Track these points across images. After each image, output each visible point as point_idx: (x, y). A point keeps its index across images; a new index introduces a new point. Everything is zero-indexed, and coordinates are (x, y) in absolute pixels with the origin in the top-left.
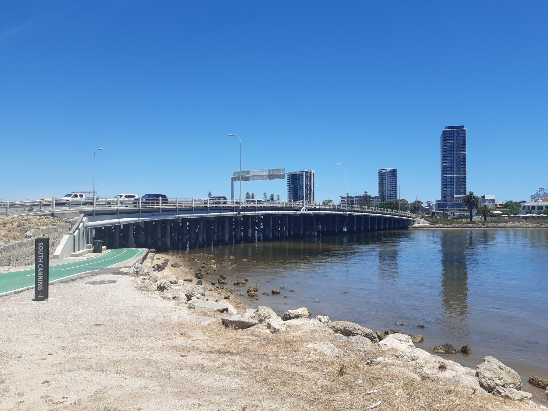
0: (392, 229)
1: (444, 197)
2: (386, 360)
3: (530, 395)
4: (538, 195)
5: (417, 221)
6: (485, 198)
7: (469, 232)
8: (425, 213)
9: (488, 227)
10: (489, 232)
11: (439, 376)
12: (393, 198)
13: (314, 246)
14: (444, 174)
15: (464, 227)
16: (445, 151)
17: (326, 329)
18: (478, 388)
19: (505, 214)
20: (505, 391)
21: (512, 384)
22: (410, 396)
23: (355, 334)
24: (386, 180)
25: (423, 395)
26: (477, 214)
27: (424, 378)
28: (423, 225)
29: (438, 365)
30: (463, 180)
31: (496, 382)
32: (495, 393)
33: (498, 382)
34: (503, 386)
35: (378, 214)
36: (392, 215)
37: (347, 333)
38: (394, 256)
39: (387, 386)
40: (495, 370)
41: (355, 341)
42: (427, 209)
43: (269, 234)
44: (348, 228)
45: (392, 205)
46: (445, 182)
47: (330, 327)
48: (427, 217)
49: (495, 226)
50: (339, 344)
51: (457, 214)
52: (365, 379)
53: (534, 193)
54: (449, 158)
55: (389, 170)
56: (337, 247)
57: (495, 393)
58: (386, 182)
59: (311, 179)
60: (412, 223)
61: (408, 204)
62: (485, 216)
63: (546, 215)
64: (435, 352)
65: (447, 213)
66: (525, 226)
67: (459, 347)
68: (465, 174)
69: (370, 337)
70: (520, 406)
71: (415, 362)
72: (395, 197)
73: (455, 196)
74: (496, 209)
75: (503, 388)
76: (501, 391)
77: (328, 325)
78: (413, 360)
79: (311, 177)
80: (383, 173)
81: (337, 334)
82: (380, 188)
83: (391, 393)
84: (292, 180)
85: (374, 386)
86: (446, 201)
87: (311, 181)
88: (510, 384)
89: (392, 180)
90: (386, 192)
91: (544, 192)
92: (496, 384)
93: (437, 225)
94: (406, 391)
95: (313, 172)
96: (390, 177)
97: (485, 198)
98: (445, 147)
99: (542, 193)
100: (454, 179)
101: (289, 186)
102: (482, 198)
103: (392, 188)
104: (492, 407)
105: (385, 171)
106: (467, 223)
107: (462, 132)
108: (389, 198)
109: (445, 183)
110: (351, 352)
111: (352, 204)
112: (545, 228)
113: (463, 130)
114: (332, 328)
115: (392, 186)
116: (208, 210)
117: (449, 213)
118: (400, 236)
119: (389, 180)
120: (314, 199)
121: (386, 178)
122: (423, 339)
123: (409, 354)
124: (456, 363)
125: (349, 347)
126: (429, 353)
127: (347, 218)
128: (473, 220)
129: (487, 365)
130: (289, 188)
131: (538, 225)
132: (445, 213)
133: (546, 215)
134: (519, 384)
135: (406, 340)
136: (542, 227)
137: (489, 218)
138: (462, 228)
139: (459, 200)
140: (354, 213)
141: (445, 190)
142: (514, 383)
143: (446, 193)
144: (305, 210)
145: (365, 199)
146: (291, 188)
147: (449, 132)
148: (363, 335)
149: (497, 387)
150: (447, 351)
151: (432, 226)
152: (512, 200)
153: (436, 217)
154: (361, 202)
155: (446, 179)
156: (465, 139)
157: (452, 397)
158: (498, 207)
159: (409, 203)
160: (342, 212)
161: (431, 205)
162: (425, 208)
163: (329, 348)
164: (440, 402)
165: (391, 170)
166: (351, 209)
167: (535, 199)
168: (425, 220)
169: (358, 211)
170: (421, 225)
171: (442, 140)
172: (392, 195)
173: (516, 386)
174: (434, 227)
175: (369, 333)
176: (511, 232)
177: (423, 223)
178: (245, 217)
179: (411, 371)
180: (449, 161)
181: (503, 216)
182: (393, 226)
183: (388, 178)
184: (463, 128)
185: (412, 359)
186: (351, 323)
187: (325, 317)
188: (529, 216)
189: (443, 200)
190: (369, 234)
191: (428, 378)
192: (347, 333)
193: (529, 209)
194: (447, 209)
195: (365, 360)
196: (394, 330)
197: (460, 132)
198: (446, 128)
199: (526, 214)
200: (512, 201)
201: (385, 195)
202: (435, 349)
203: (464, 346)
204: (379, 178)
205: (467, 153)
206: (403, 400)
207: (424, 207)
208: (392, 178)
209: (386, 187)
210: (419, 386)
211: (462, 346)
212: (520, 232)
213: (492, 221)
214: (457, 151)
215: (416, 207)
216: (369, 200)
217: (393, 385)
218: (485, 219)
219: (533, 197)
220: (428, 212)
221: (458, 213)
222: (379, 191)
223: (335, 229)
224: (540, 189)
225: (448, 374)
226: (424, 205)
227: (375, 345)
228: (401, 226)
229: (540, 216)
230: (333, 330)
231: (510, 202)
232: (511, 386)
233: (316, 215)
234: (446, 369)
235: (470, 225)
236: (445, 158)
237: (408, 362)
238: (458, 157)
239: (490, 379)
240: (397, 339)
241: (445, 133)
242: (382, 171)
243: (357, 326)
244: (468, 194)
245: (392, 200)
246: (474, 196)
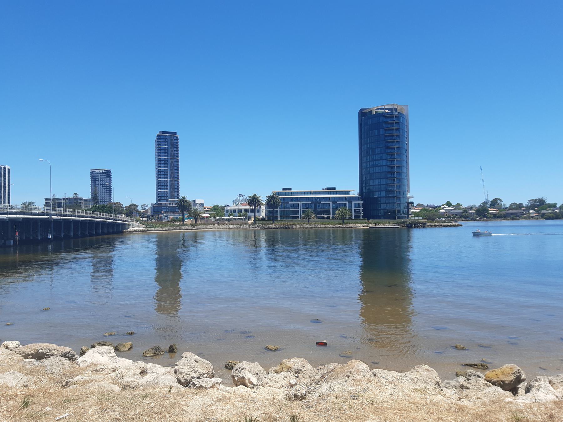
0: (100, 235)
1: (159, 200)
2: (85, 377)
3: (220, 380)
4: (238, 200)
5: (132, 225)
6: (196, 202)
7: (182, 234)
8: (140, 216)
9: (198, 229)
10: (199, 234)
11: (139, 382)
12: (107, 198)
13: (11, 258)
14: (158, 178)
15: (176, 230)
16: (160, 156)
17: (13, 356)
18: (176, 385)
19: (212, 217)
20: (200, 382)
21: (206, 373)
22: (104, 411)
23: (50, 356)
24: (100, 181)
25: (119, 406)
26: (189, 217)
27: (125, 387)
28: (138, 229)
29: (139, 371)
31: (192, 376)
32: (191, 386)
33: (194, 375)
34: (198, 378)
35: (89, 218)
36: (105, 219)
37: (39, 356)
38: (109, 262)
39: (80, 406)
40: (191, 364)
41: (49, 364)
42: (143, 213)
44: (53, 234)
45: (106, 208)
46: (159, 186)
47: (18, 354)
48: (142, 220)
49: (204, 228)
50: (29, 371)
51: (171, 217)
52: (56, 404)
53: (235, 198)
54: (163, 162)
55: (103, 171)
56: (41, 257)
57: (191, 386)
58: (100, 184)
59: (5, 176)
60: (127, 227)
61: (123, 207)
62: (196, 219)
63: (244, 218)
64: (144, 357)
65: (162, 217)
66: (228, 227)
67: (165, 347)
68: (178, 178)
69: (69, 356)
70: (209, 393)
71: (116, 372)
73: (169, 200)
74: (205, 213)
75: (198, 380)
76: (196, 383)
77: (16, 352)
78: (114, 371)
79: (5, 174)
80: (96, 174)
81: (27, 360)
82: (93, 190)
83: (84, 412)
85: (65, 410)
86: (161, 204)
87: (5, 189)
88: (204, 374)
89: (105, 181)
90: (100, 194)
91: (243, 197)
92: (192, 377)
93: (152, 229)
94: (101, 406)
95: (7, 167)
96: (103, 178)
97: (196, 202)
98: (159, 151)
99: (241, 198)
100: (168, 183)
102: (193, 202)
103: (106, 190)
104: (185, 401)
105: (98, 171)
106: (180, 225)
107: (175, 138)
108: (104, 201)
109: (160, 187)
110: (44, 377)
111: (60, 207)
112: (243, 228)
113: (176, 136)
114: (20, 354)
115: (106, 187)
117: (163, 217)
118: (114, 241)
120: (9, 200)
121: (100, 180)
122: (132, 346)
123: (110, 366)
124: (157, 365)
125: (41, 371)
126: (132, 361)
127: (53, 223)
128: (185, 223)
129: (184, 361)
131: (238, 226)
132: (160, 216)
133: (244, 218)
134: (211, 372)
135: (107, 352)
136: (241, 228)
137: (199, 221)
138: (175, 231)
139: (173, 204)
140: (61, 217)
141: (160, 194)
142: (208, 373)
143: (161, 197)
145: (75, 202)
147: (163, 137)
148: (60, 355)
149: (193, 380)
150: (155, 353)
151: (147, 229)
152: (218, 204)
153: (151, 221)
154: (70, 205)
155: (161, 183)
156: (178, 145)
157: (148, 401)
158: (207, 211)
159: (124, 206)
160: (47, 217)
161: (147, 208)
162: (141, 211)
163: (14, 378)
164: (136, 409)
165: (104, 171)
166: (57, 212)
167: (236, 204)
168: (140, 223)
169: (66, 215)
170: (136, 229)
171: (156, 144)
172: (106, 198)
173: (210, 375)
174: (149, 231)
175: (67, 352)
176: (217, 234)
177: (138, 227)
179: (111, 383)
181: (211, 219)
182: (106, 231)
183: (102, 179)
184: (176, 134)
185: (113, 370)
186: (45, 344)
187: (13, 342)
188: (231, 219)
189: (158, 203)
190: (80, 240)
191: (129, 386)
192: (39, 356)
193: (231, 212)
194: (162, 212)
195: (61, 382)
196: (101, 343)
197: (173, 138)
198: (160, 132)
199: (229, 217)
201: (98, 197)
202: (143, 354)
203: (171, 346)
204: (92, 178)
205: (180, 158)
206: (97, 416)
207: (139, 210)
208: (105, 179)
209: (99, 189)
210: (115, 398)
211: (170, 346)
212: (224, 233)
213: (201, 224)
215: (131, 211)
217: (87, 403)
218: (196, 222)
219: (234, 202)
220: (144, 215)
221: (172, 216)
222: (92, 193)
223: (37, 236)
225: (148, 378)
226: (140, 209)
227: (73, 364)
228: (116, 230)
229: (239, 218)
230: (23, 356)
231: (217, 206)
232: (205, 376)
233: (10, 220)
234: (147, 373)
235: (183, 228)
236: (160, 162)
237: (109, 374)
238: (172, 162)
239: (186, 374)
240: (98, 352)
241: (159, 137)
243: (52, 346)
244: (181, 198)
245: (106, 203)
246: (186, 200)
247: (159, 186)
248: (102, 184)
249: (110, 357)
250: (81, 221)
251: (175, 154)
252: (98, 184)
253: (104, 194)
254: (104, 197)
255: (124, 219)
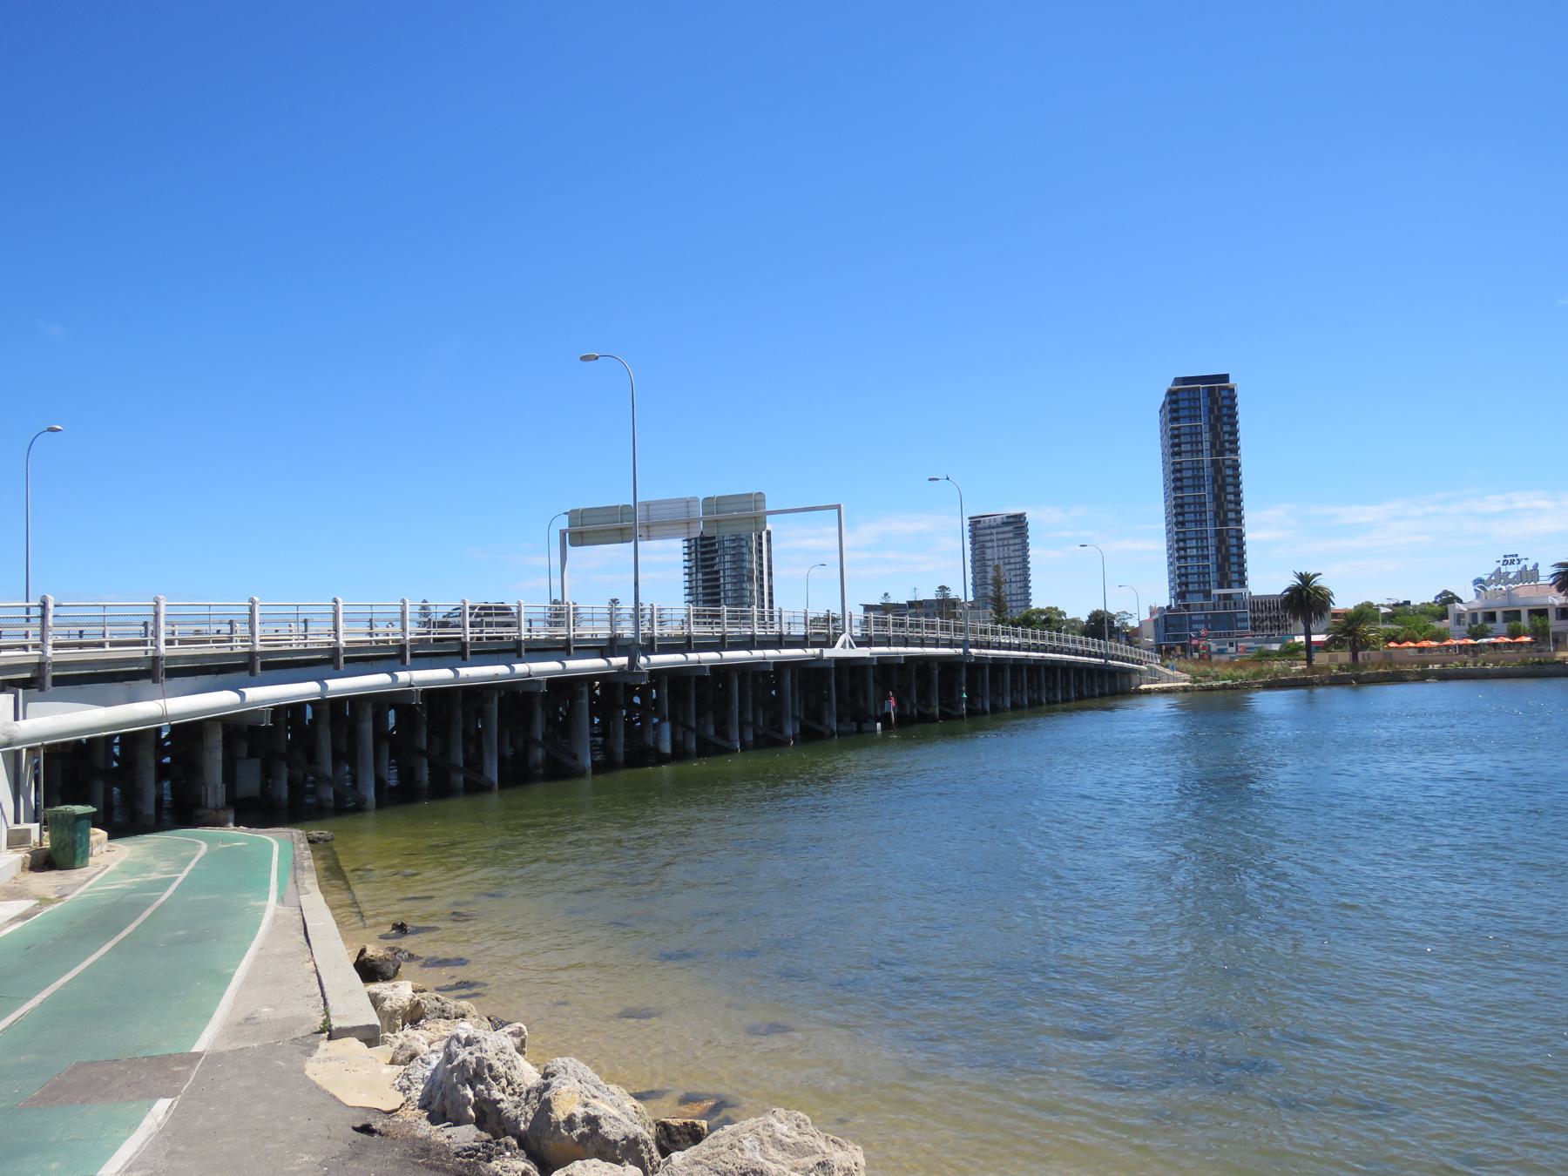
1: (1180, 596)
12: (1019, 598)
30: (1234, 541)
43: (657, 740)
54: (1189, 473)
59: (761, 551)
60: (1135, 679)
65: (1209, 646)
72: (1022, 597)
80: (984, 528)
84: (699, 554)
87: (761, 558)
89: (1012, 548)
91: (1520, 567)
101: (690, 574)
103: (1013, 573)
107: (1225, 393)
115: (1013, 566)
116: (468, 656)
119: (1004, 550)
130: (690, 581)
144: (848, 645)
145: (944, 606)
146: (697, 580)
147: (1186, 395)
165: (1008, 517)
172: (1014, 598)
178: (657, 674)
180: (1190, 482)
198: (1178, 381)
200: (1371, 603)
208: (1011, 542)
214: (1214, 452)
216: (952, 613)
224: (1505, 556)
229: (1478, 645)
242: (980, 521)
247: (1178, 550)
248: (1001, 556)
249: (439, 929)
250: (1011, 662)
251: (1227, 445)
252: (991, 557)
253: (1010, 586)
254: (1011, 594)
255: (1129, 655)
